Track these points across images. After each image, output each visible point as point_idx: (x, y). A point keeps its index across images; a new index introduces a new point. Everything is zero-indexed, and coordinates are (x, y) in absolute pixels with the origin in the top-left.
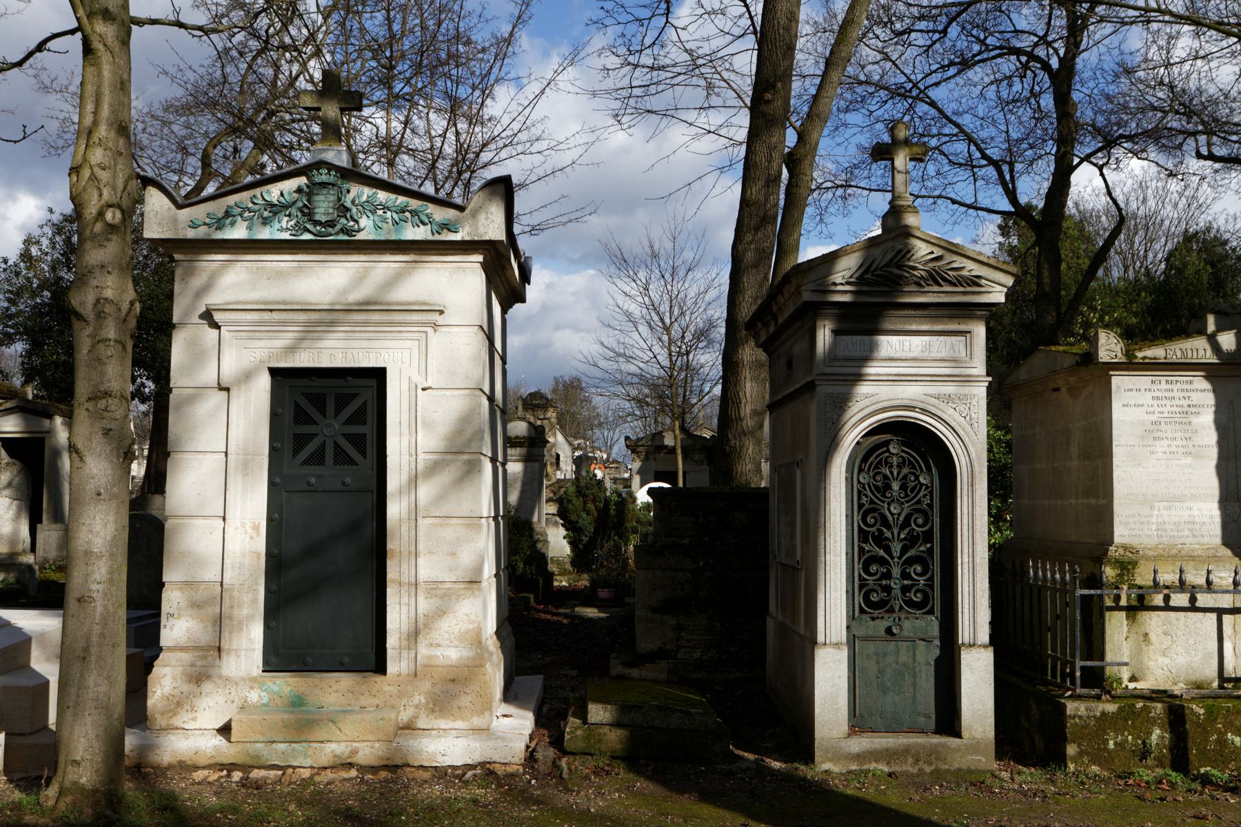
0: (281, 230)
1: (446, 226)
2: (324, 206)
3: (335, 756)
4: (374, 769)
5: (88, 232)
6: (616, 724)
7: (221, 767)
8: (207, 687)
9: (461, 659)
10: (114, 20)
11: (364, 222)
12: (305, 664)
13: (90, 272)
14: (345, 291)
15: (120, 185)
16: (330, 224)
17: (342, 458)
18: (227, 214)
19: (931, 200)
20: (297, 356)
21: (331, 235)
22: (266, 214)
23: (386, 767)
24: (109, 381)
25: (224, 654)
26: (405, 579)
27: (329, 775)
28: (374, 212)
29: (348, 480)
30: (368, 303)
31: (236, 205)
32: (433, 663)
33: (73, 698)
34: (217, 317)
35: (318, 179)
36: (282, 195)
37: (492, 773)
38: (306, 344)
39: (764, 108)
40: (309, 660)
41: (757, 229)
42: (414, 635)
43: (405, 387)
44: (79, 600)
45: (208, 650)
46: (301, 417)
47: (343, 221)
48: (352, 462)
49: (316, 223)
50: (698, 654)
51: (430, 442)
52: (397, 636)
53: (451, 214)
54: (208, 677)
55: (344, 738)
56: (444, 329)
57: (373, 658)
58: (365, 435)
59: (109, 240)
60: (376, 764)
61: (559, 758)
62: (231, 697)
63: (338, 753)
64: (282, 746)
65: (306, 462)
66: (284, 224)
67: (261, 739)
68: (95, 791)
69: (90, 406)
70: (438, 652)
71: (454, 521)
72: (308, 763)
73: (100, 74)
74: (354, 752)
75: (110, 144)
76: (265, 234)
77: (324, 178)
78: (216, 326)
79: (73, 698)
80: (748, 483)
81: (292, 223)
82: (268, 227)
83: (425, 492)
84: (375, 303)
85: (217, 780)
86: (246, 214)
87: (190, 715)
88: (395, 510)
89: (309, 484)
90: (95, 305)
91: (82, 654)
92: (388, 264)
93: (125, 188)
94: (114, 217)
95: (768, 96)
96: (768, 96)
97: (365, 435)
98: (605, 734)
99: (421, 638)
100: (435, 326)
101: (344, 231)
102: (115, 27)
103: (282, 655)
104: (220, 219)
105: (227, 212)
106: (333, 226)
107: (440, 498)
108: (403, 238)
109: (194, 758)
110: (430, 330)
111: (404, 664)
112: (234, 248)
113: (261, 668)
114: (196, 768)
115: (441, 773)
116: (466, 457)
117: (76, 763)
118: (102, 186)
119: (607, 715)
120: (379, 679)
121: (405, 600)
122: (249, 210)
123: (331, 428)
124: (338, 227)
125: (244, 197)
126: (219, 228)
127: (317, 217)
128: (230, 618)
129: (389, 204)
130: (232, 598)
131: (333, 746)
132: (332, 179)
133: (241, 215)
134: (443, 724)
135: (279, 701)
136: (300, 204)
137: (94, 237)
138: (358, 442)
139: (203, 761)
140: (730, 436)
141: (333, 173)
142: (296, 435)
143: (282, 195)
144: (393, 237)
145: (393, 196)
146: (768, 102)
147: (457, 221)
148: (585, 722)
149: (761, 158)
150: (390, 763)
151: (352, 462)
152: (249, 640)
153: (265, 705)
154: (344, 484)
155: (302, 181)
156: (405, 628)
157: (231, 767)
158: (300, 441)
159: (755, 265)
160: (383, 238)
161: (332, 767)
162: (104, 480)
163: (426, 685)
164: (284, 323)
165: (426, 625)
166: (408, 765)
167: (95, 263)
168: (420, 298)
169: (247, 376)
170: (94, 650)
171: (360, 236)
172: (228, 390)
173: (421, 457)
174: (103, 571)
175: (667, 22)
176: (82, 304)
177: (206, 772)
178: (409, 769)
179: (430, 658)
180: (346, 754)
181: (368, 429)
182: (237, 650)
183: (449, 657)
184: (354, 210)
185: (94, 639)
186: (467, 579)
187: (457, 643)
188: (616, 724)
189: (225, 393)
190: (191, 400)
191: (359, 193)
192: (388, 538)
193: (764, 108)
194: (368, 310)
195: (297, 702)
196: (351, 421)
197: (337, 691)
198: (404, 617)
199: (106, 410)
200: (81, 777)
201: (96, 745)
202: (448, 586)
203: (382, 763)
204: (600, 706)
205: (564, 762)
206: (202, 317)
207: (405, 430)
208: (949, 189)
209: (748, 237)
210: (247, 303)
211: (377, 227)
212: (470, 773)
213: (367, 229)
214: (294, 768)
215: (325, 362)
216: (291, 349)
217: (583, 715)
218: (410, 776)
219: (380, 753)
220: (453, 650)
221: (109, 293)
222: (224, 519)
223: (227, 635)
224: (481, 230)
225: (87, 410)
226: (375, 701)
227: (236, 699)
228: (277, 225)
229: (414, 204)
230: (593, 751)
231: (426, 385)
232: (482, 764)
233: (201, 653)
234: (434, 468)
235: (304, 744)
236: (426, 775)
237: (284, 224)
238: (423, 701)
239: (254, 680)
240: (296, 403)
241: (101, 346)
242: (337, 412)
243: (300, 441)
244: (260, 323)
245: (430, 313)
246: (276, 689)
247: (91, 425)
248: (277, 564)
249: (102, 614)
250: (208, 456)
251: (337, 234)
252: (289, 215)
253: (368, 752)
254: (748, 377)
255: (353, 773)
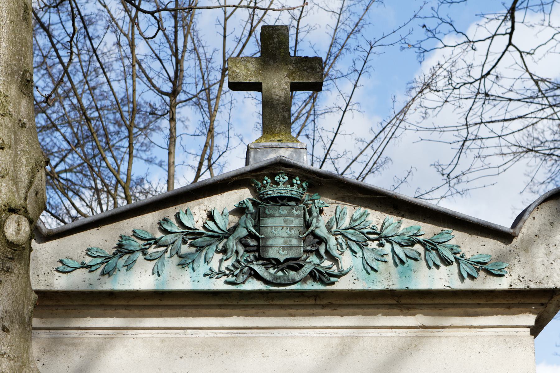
0: (210, 275)
1: (482, 267)
2: (282, 234)
11: (347, 260)
16: (293, 264)
18: (121, 249)
35: (272, 191)
36: (211, 217)
47: (314, 259)
49: (275, 263)
59: (8, 270)
77: (283, 190)
86: (152, 250)
93: (31, 183)
105: (120, 246)
106: (297, 268)
112: (127, 307)
124: (307, 269)
127: (272, 254)
129: (388, 232)
132: (295, 191)
133: (144, 251)
143: (211, 217)
145: (393, 219)
147: (502, 258)
155: (244, 194)
160: (379, 286)
171: (342, 285)
175: (510, 43)
184: (332, 241)
213: (353, 273)
229: (428, 230)
237: (215, 265)
251: (304, 280)
252: (224, 251)
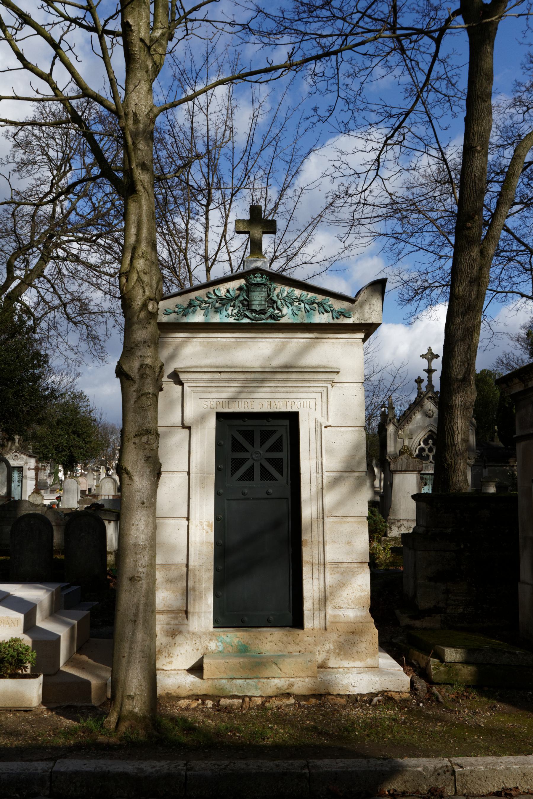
0: (228, 316)
1: (343, 314)
2: (258, 299)
3: (277, 688)
4: (305, 697)
5: (136, 318)
6: (466, 662)
7: (196, 697)
8: (179, 639)
9: (357, 617)
10: (148, 170)
11: (285, 310)
12: (243, 621)
13: (136, 346)
14: (269, 358)
15: (155, 285)
16: (263, 312)
17: (266, 475)
18: (190, 305)
19: (504, 294)
20: (236, 404)
21: (263, 320)
22: (217, 305)
23: (313, 696)
24: (149, 423)
25: (190, 616)
26: (316, 561)
27: (277, 702)
28: (292, 304)
29: (271, 491)
30: (286, 367)
31: (196, 298)
32: (337, 620)
33: (127, 650)
34: (182, 377)
35: (254, 281)
36: (228, 291)
37: (391, 699)
38: (243, 395)
39: (466, 232)
40: (246, 619)
41: (464, 314)
42: (324, 601)
43: (312, 425)
44: (131, 579)
45: (178, 613)
46: (237, 447)
47: (271, 310)
48: (273, 478)
49: (255, 311)
50: (461, 610)
51: (332, 463)
52: (311, 602)
53: (343, 305)
54: (180, 632)
55: (284, 675)
56: (338, 385)
57: (289, 616)
58: (282, 459)
59: (149, 323)
60: (307, 693)
61: (431, 687)
62: (196, 647)
63: (280, 685)
64: (240, 682)
65: (240, 479)
66: (230, 312)
67: (225, 676)
68: (145, 718)
69: (136, 440)
70: (340, 612)
71: (349, 519)
72: (258, 693)
73: (140, 207)
74: (291, 685)
75: (149, 257)
76: (217, 319)
77: (258, 280)
78: (181, 383)
79: (127, 650)
80: (460, 489)
81: (235, 311)
82: (219, 314)
83: (330, 499)
84: (291, 367)
85: (197, 707)
86: (203, 305)
87: (168, 660)
88: (308, 512)
89: (243, 494)
90: (139, 369)
91: (133, 618)
92: (297, 341)
93: (157, 287)
94: (153, 307)
95: (469, 224)
96: (469, 224)
97: (282, 459)
98: (460, 670)
99: (328, 604)
100: (333, 383)
101: (272, 317)
102: (148, 175)
103: (224, 618)
104: (185, 309)
107: (340, 504)
108: (312, 321)
109: (177, 691)
110: (329, 386)
111: (317, 622)
113: (212, 626)
114: (179, 698)
115: (354, 700)
116: (356, 474)
117: (131, 698)
118: (145, 286)
119: (458, 656)
120: (300, 632)
121: (316, 575)
122: (206, 302)
123: (258, 455)
124: (268, 314)
125: (201, 293)
126: (185, 315)
127: (254, 307)
128: (194, 589)
129: (303, 298)
130: (195, 575)
131: (276, 681)
132: (264, 281)
133: (200, 306)
134: (346, 663)
135: (230, 649)
136: (241, 298)
137: (139, 322)
138: (277, 464)
139: (184, 693)
140: (448, 457)
141: (264, 276)
142: (233, 460)
143: (228, 291)
144: (306, 321)
145: (305, 293)
146: (469, 229)
148: (442, 661)
149: (464, 266)
150: (316, 692)
151: (273, 478)
152: (205, 605)
153: (220, 652)
154: (268, 493)
155: (242, 282)
156: (316, 595)
157: (204, 697)
158: (236, 464)
159: (463, 340)
160: (298, 322)
161: (276, 696)
162: (146, 493)
163: (334, 636)
164: (229, 381)
165: (331, 594)
166: (330, 694)
167: (140, 340)
168: (322, 364)
169: (202, 419)
170: (141, 615)
171: (283, 321)
172: (189, 428)
173: (325, 474)
174: (146, 559)
175: (377, 175)
176: (131, 368)
177: (187, 701)
178: (330, 697)
179: (335, 616)
180: (285, 687)
181: (284, 455)
182: (198, 613)
183: (348, 616)
184: (279, 302)
185: (141, 607)
186: (359, 560)
187: (353, 606)
188: (466, 662)
189: (186, 431)
190: (167, 434)
191: (281, 290)
192: (303, 532)
193: (466, 232)
194: (287, 372)
195: (243, 650)
196: (272, 449)
197: (271, 642)
198: (316, 588)
199: (147, 443)
200: (135, 708)
201: (144, 684)
202: (345, 565)
203: (311, 693)
204: (452, 650)
205: (435, 689)
206: (169, 377)
207: (313, 455)
208: (514, 287)
209: (458, 320)
210: (201, 367)
211: (294, 314)
212: (375, 699)
213: (287, 315)
214: (250, 697)
215: (256, 408)
216: (233, 400)
217: (441, 658)
218: (332, 702)
219: (309, 686)
220: (351, 611)
221: (148, 361)
222: (188, 519)
223: (192, 601)
224: (366, 316)
225: (135, 443)
226: (298, 648)
227: (200, 648)
228: (224, 313)
229: (320, 298)
230: (452, 682)
231: (328, 424)
232: (382, 693)
233: (173, 615)
234: (336, 481)
235: (255, 680)
236: (343, 701)
238: (332, 647)
239: (212, 634)
240: (233, 437)
241: (144, 398)
242: (262, 443)
243: (236, 464)
244: (212, 381)
245: (329, 374)
246: (228, 640)
247: (137, 454)
248: (223, 550)
249: (146, 589)
250: (176, 475)
251: (267, 319)
252: (234, 306)
253: (301, 685)
254: (459, 416)
255: (292, 701)
